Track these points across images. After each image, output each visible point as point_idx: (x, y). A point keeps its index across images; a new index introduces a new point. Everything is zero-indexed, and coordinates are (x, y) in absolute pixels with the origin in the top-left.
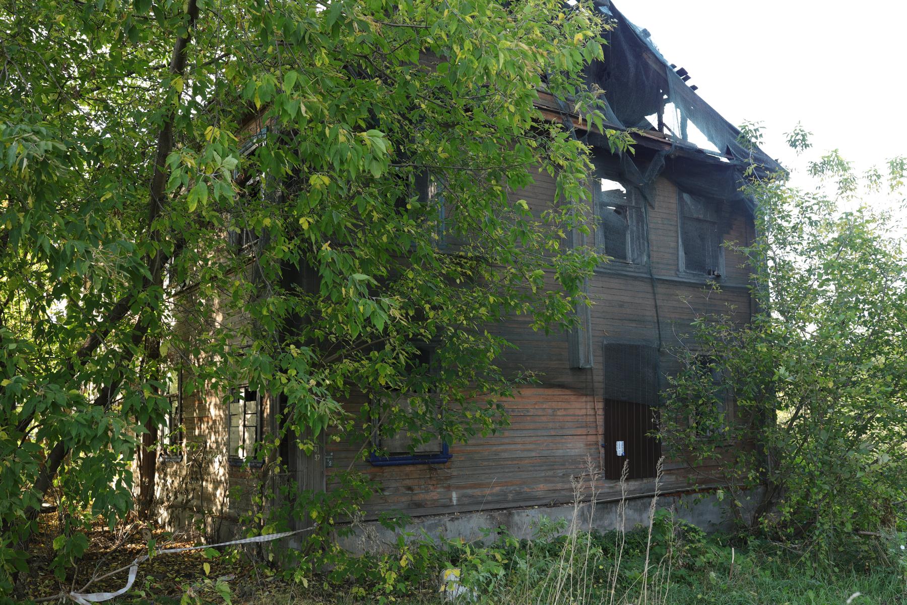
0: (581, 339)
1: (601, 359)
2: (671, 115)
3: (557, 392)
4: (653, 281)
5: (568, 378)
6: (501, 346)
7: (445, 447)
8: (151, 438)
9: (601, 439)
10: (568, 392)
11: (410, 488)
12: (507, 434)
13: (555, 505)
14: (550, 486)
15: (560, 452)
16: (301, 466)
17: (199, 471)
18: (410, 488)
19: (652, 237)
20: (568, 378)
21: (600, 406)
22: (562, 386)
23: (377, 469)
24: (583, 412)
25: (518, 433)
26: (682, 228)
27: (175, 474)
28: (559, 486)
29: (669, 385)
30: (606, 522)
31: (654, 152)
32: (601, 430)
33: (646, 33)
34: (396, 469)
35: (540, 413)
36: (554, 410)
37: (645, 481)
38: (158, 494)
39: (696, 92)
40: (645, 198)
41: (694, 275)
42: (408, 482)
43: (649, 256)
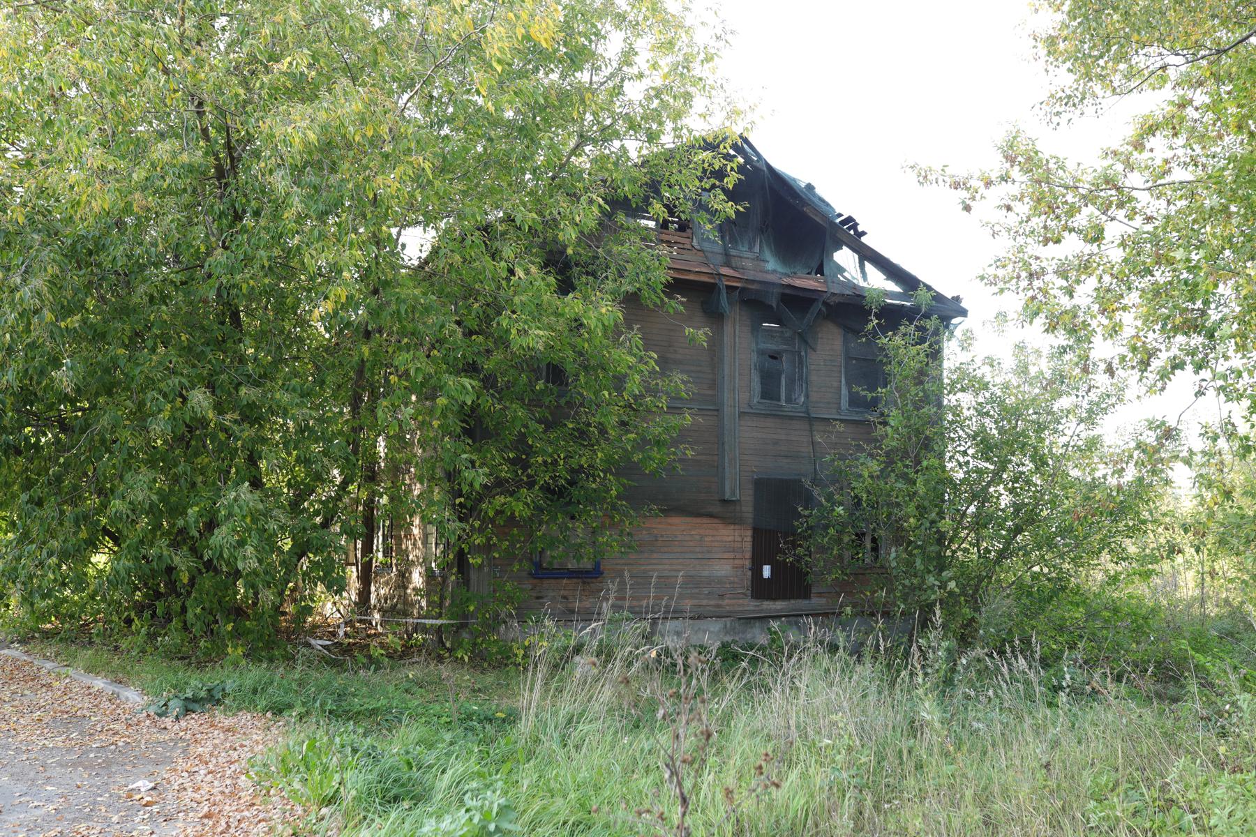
0: (727, 474)
1: (751, 492)
2: (845, 257)
3: (705, 520)
4: (810, 420)
5: (717, 509)
6: (624, 485)
7: (598, 565)
8: (368, 548)
9: (748, 563)
10: (716, 521)
11: (565, 597)
12: (655, 555)
13: (699, 618)
14: (696, 602)
15: (706, 573)
16: (473, 576)
17: (404, 577)
18: (565, 597)
19: (813, 378)
20: (717, 509)
21: (749, 533)
22: (710, 516)
23: (536, 581)
24: (731, 538)
25: (666, 556)
26: (846, 368)
27: (387, 583)
28: (705, 602)
29: (800, 516)
30: (749, 636)
31: (814, 300)
32: (748, 555)
33: (810, 187)
34: (553, 581)
35: (688, 538)
36: (702, 536)
37: (793, 601)
38: (372, 602)
39: (864, 239)
40: (806, 342)
41: (857, 413)
42: (566, 593)
43: (807, 396)
